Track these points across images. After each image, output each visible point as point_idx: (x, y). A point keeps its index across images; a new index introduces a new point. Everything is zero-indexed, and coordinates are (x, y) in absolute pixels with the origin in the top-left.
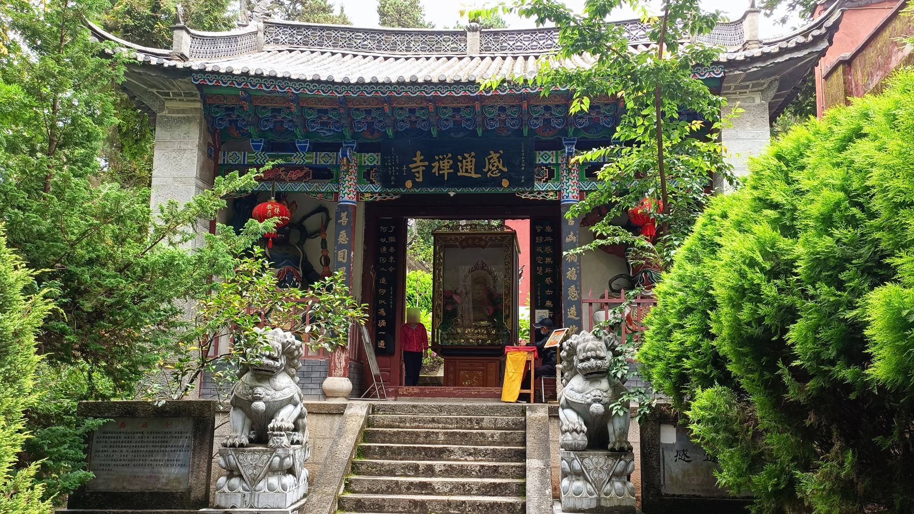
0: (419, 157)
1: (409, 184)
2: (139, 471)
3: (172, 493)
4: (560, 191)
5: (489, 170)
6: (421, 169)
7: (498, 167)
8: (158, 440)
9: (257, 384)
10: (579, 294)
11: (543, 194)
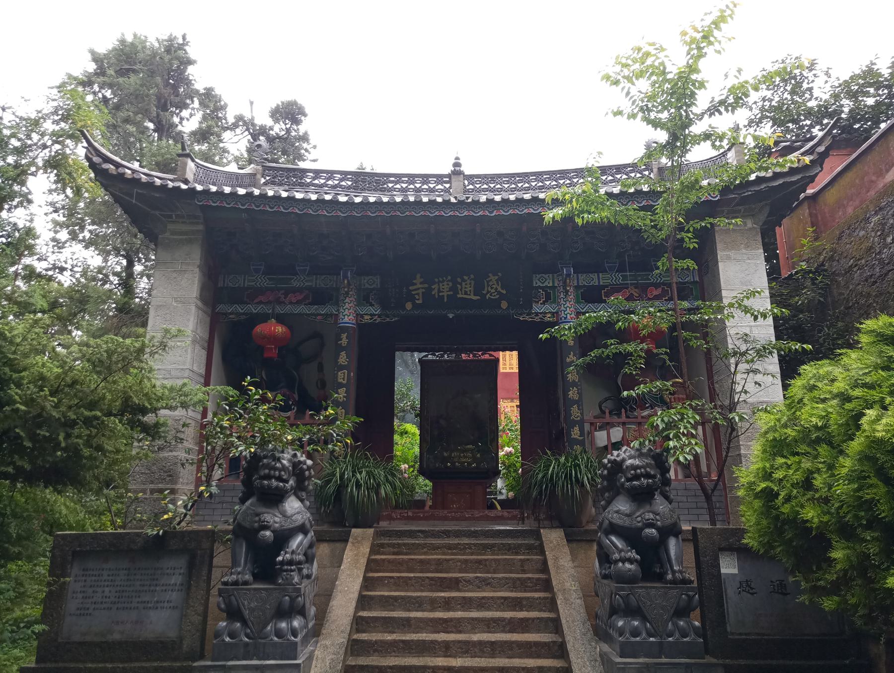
0: (418, 280)
1: (409, 306)
4: (557, 313)
5: (488, 292)
6: (420, 291)
7: (496, 289)
9: (264, 510)
10: (582, 414)
11: (541, 316)
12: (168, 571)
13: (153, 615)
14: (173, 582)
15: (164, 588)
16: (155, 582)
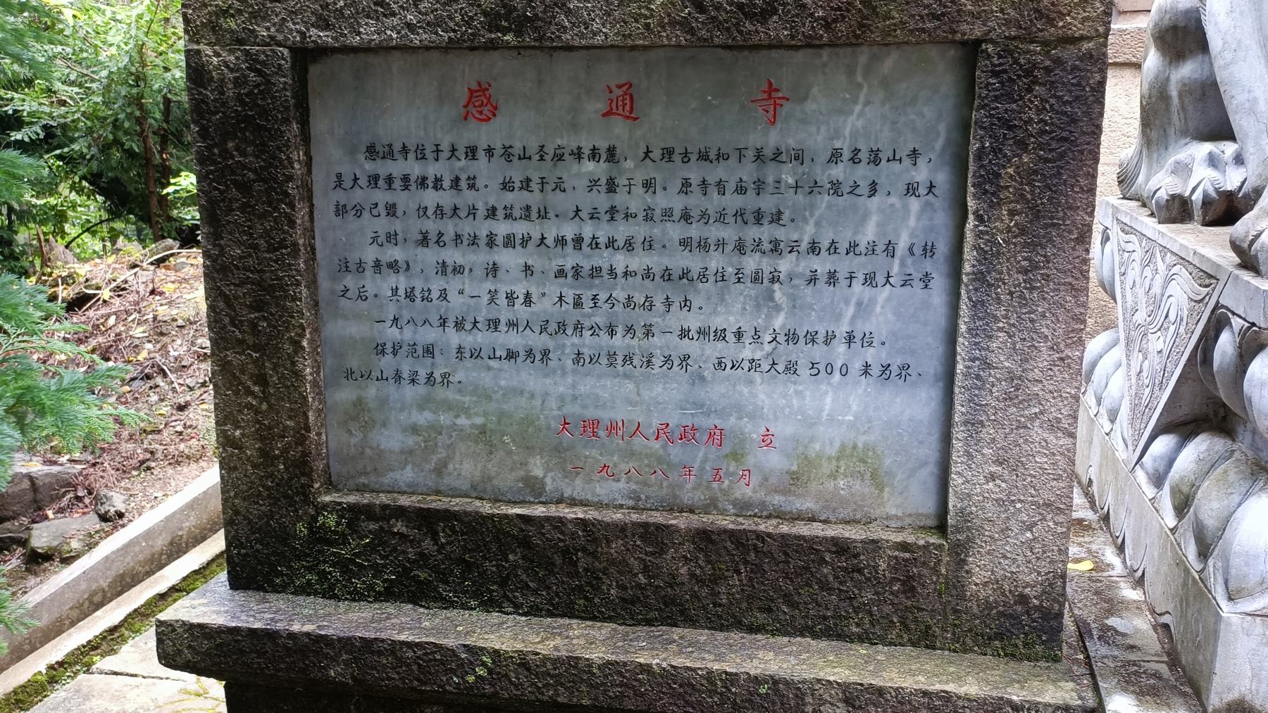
2: (612, 396)
3: (841, 547)
8: (714, 201)
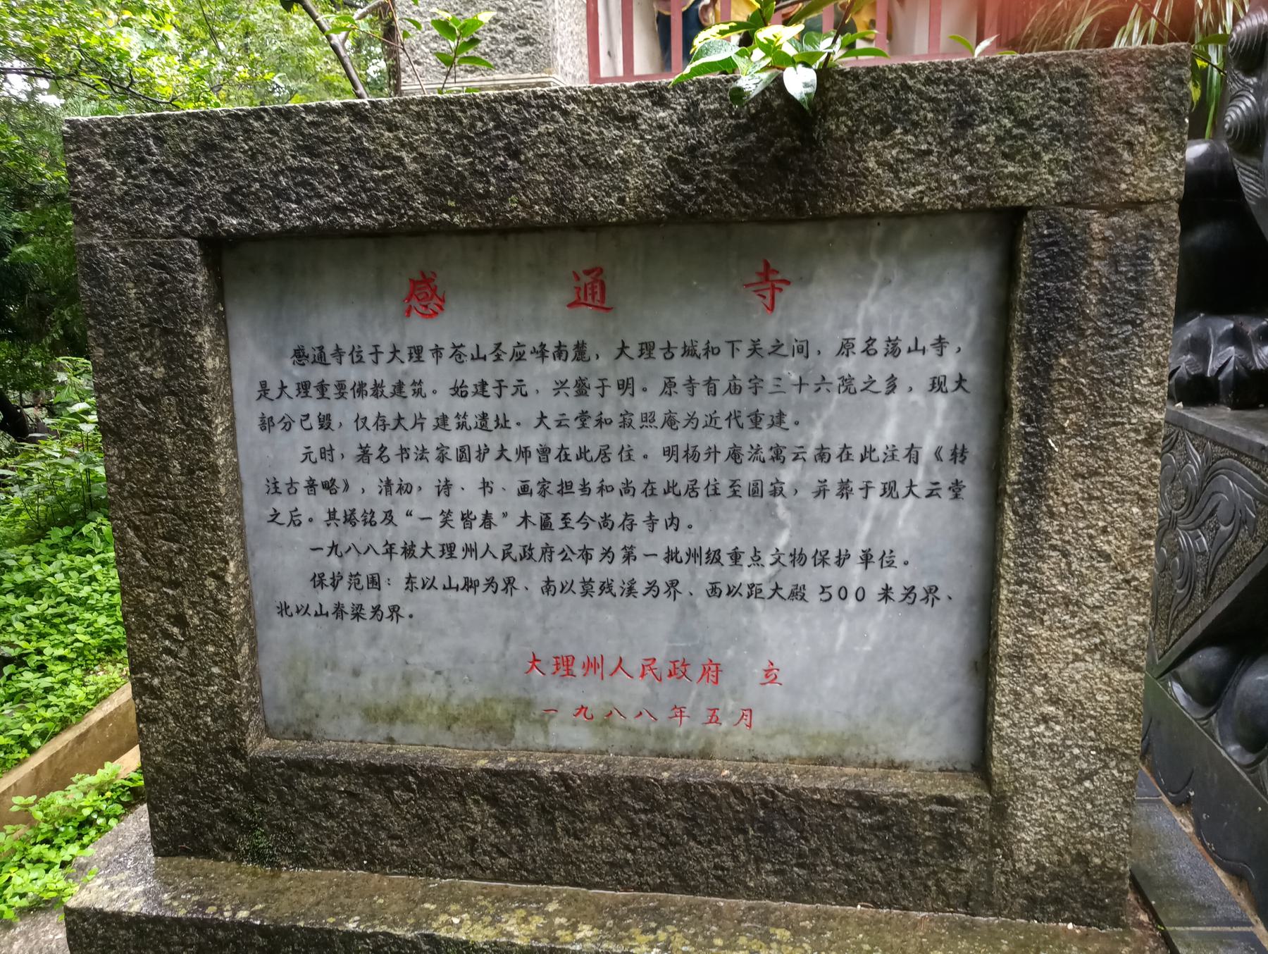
12: (848, 366)
13: (780, 633)
14: (888, 435)
15: (832, 473)
16: (765, 437)
